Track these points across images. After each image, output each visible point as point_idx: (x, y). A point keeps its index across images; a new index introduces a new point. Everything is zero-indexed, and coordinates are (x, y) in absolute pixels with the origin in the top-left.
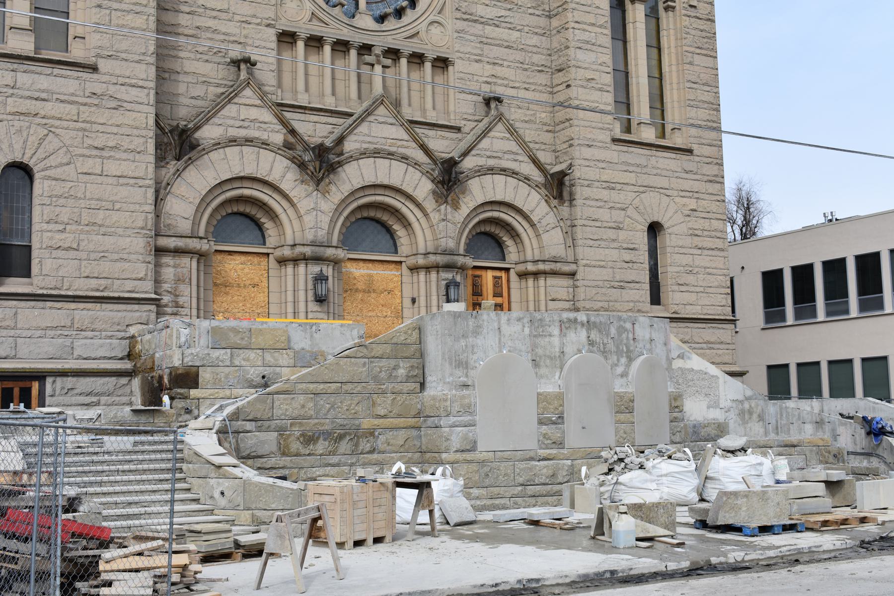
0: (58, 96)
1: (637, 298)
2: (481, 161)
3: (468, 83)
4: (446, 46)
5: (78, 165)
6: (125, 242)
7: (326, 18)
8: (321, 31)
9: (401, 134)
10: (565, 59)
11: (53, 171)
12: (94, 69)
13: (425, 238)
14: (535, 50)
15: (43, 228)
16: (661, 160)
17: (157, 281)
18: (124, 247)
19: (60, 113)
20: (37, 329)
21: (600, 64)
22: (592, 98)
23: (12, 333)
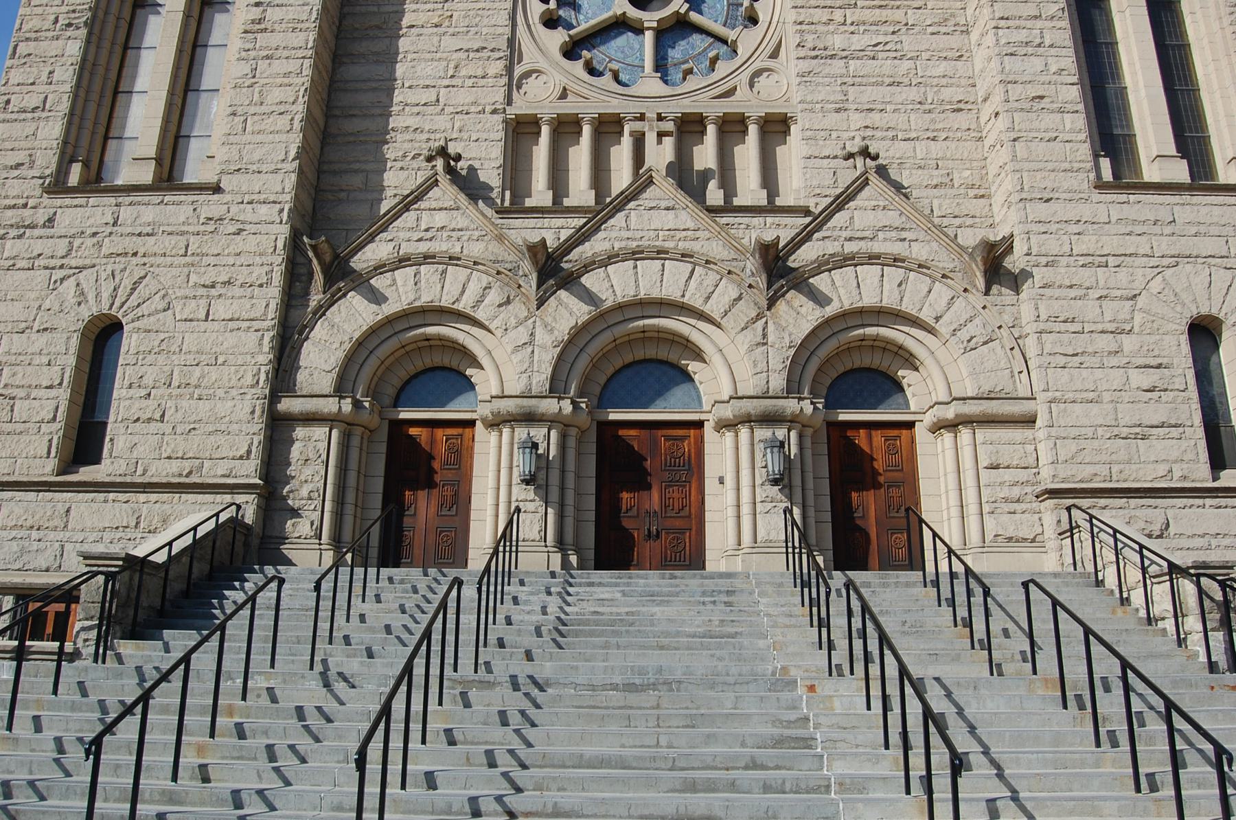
0: (166, 228)
2: (831, 248)
4: (784, 99)
5: (177, 310)
6: (224, 408)
7: (585, 91)
12: (217, 189)
13: (368, 356)
14: (944, 81)
15: (122, 396)
16: (1204, 210)
18: (223, 414)
22: (1043, 126)
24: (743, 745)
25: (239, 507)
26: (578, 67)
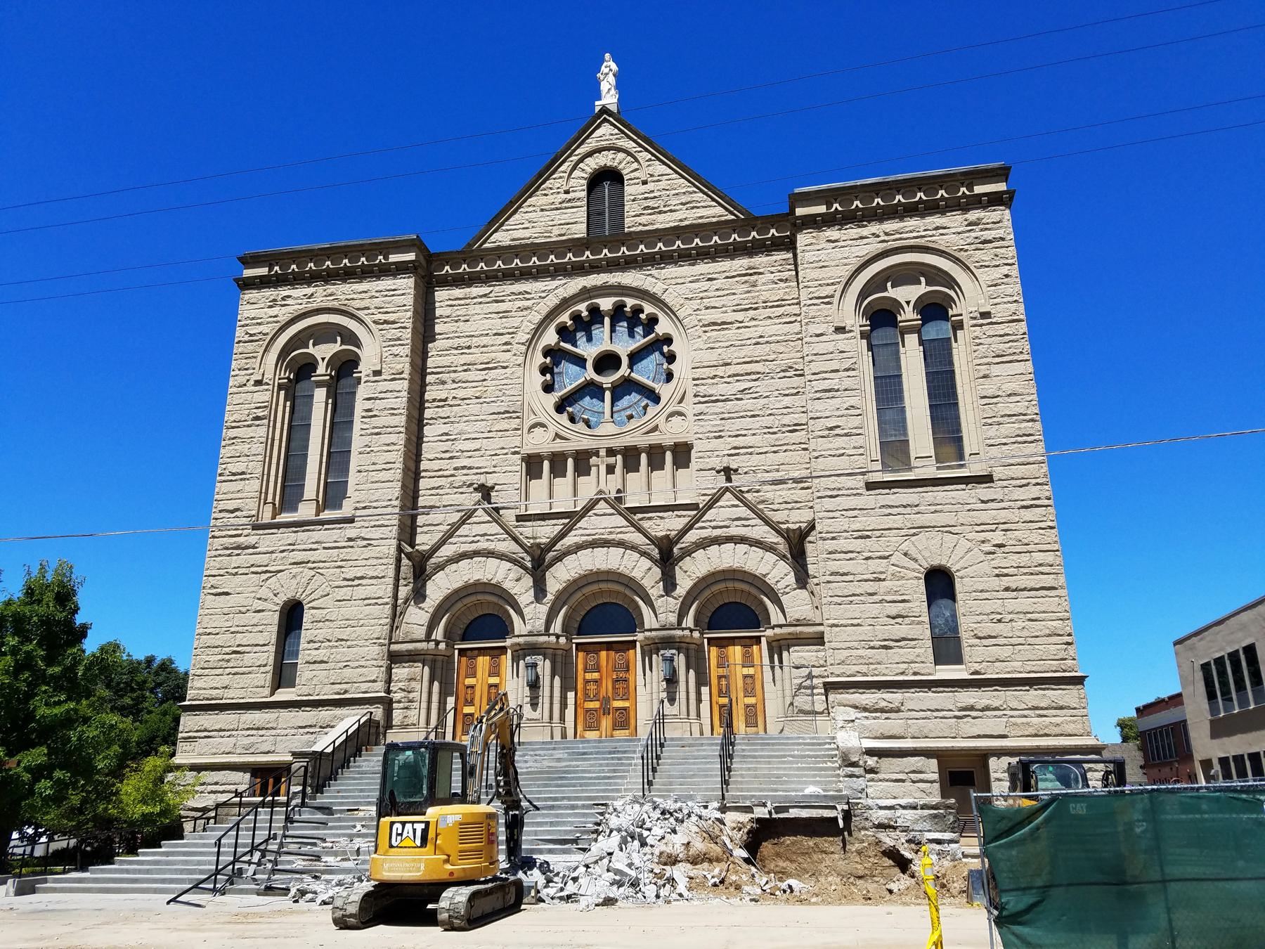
1: (912, 658)
3: (707, 460)
8: (561, 447)
9: (620, 521)
14: (785, 411)
17: (389, 681)
21: (847, 409)
24: (1140, 785)
25: (371, 713)
26: (563, 419)
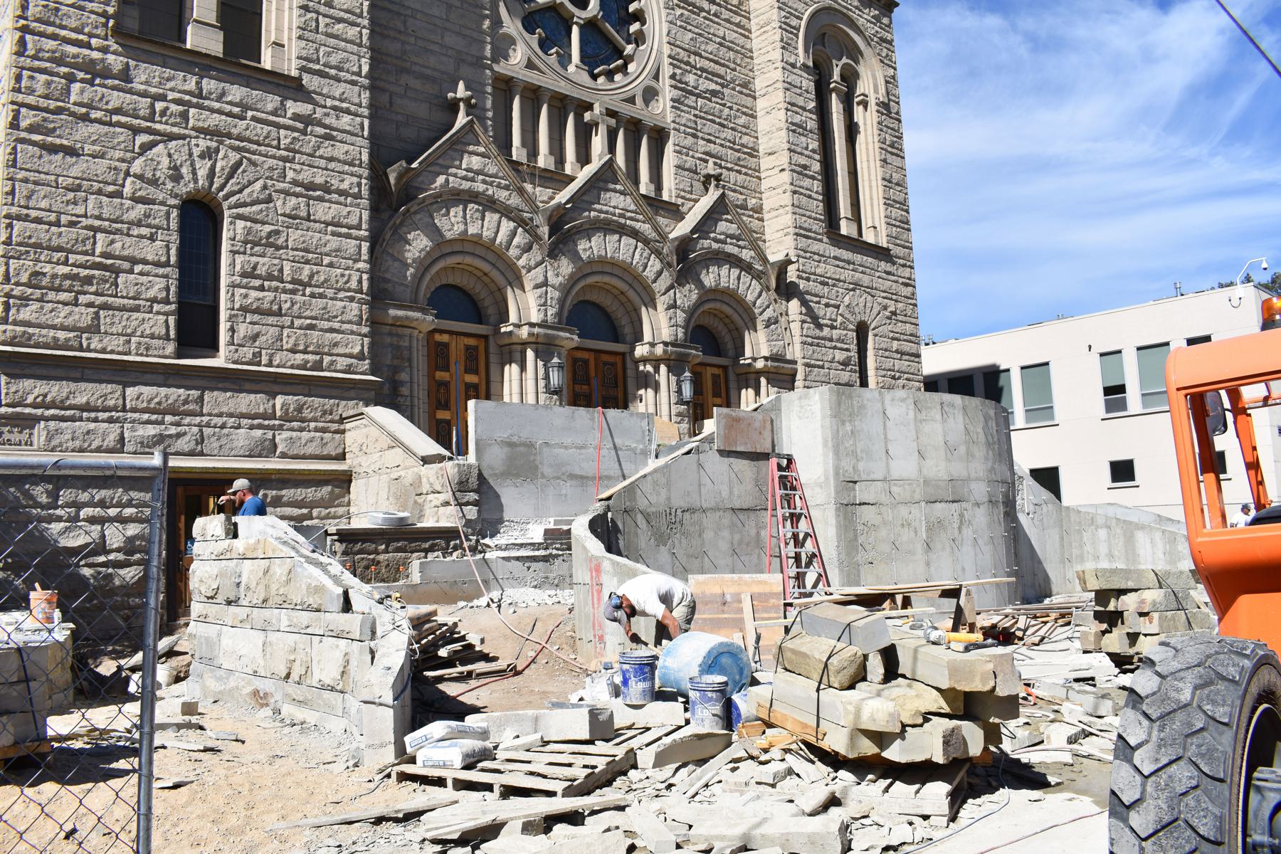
5: (279, 203)
10: (777, 141)
11: (248, 209)
19: (256, 135)
20: (231, 415)
23: (198, 419)
